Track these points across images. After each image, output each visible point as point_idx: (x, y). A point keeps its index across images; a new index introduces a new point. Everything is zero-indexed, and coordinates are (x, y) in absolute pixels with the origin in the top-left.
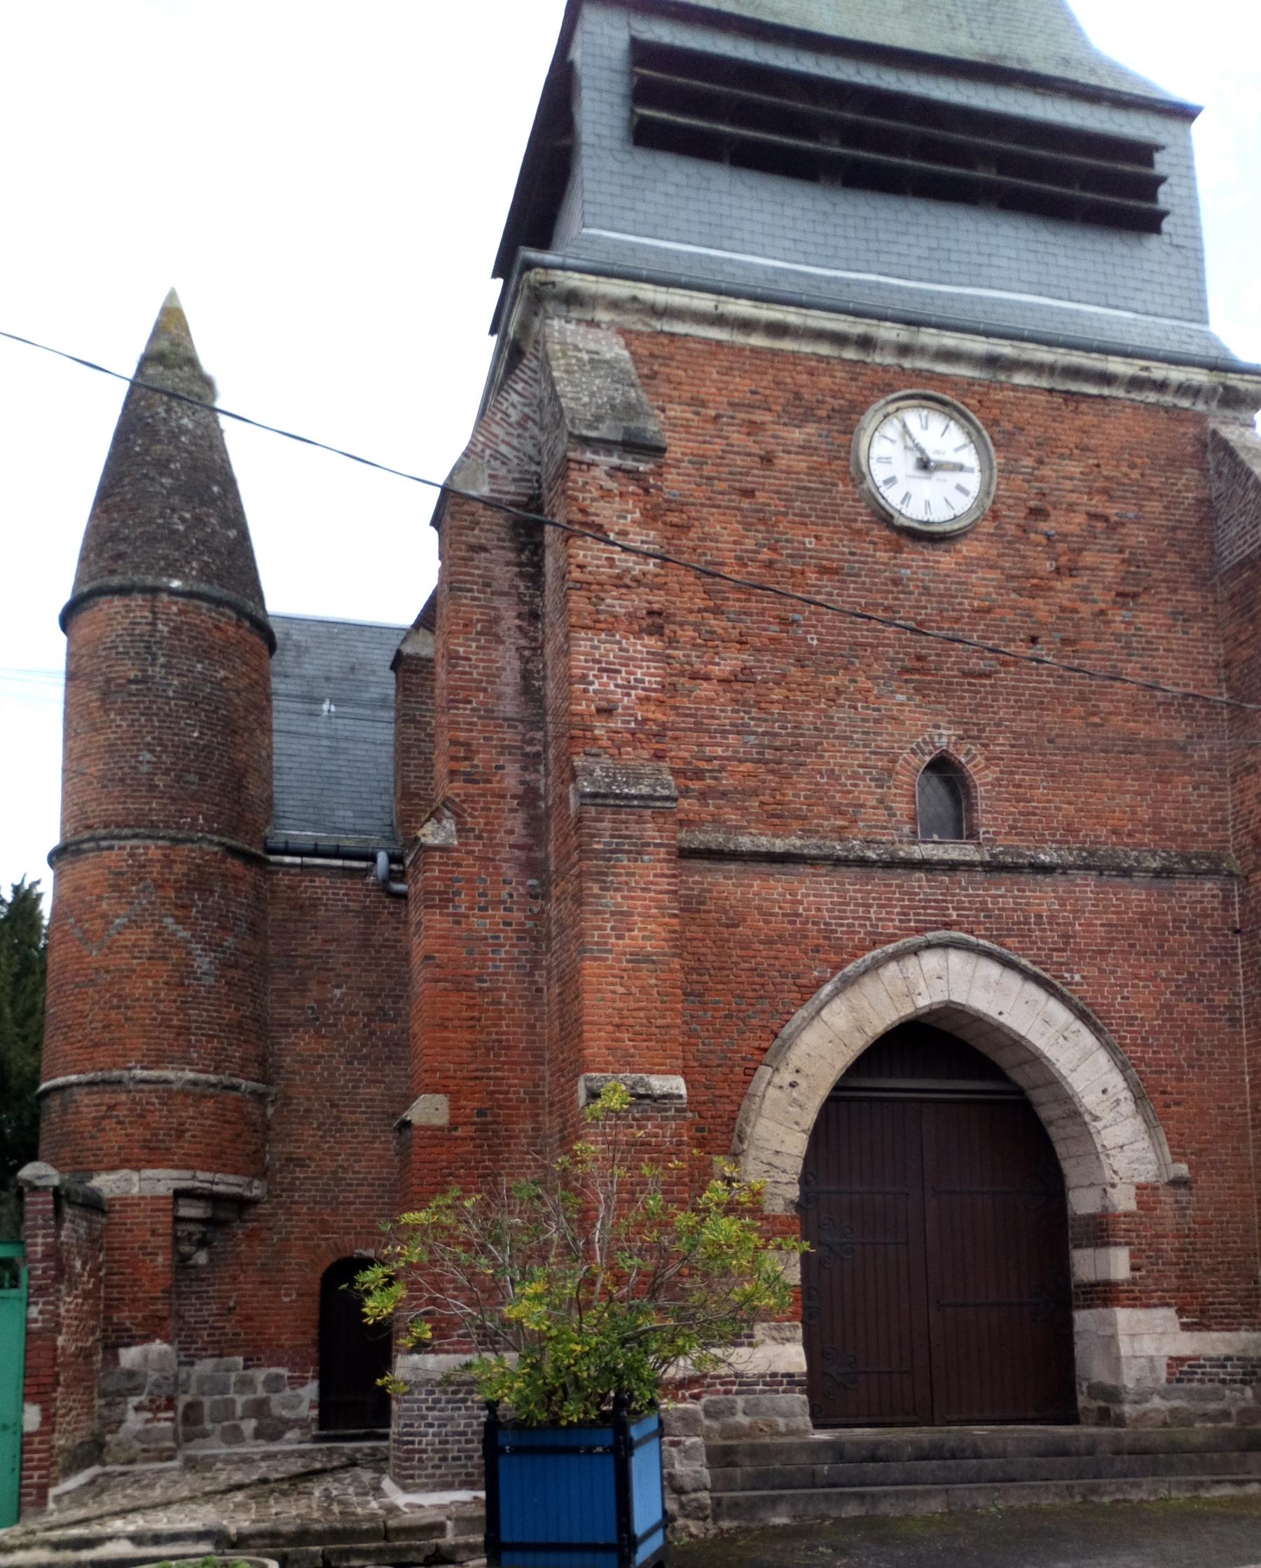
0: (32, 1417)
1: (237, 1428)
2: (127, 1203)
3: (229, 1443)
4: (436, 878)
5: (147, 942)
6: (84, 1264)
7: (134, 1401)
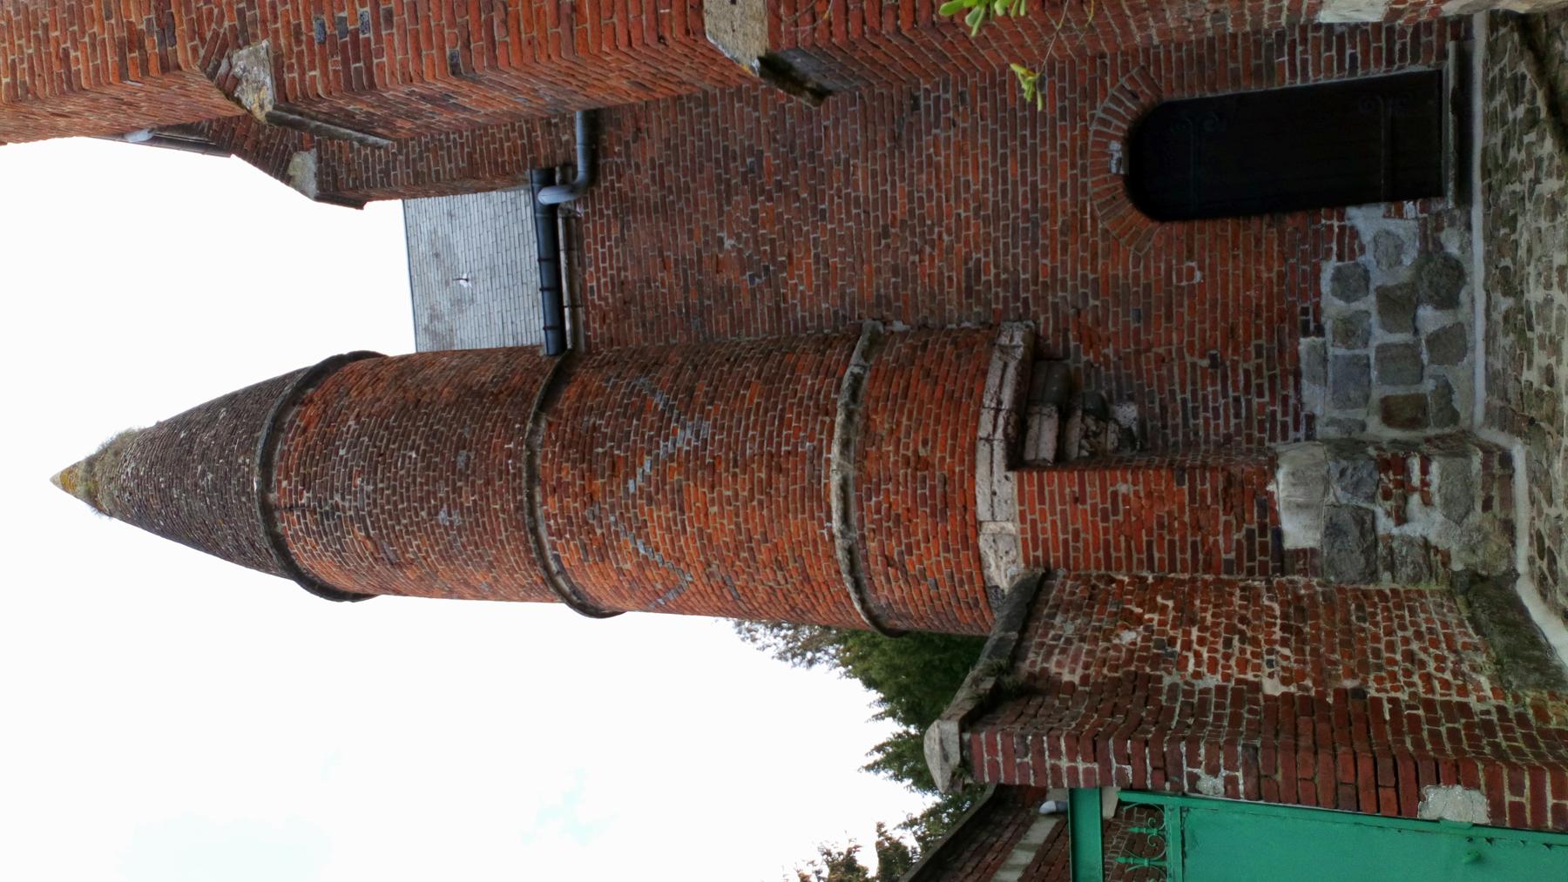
0: (1453, 804)
1: (1434, 340)
2: (1031, 540)
3: (1464, 350)
4: (325, 73)
5: (662, 513)
6: (1134, 621)
7: (1385, 525)
